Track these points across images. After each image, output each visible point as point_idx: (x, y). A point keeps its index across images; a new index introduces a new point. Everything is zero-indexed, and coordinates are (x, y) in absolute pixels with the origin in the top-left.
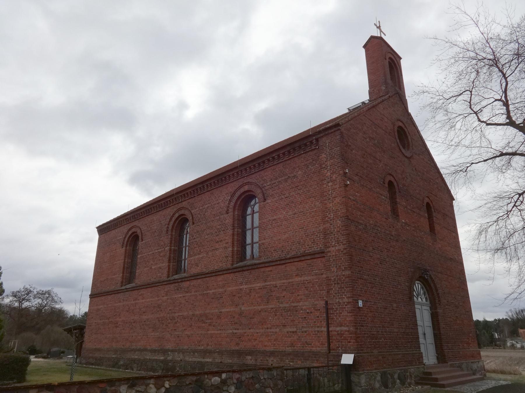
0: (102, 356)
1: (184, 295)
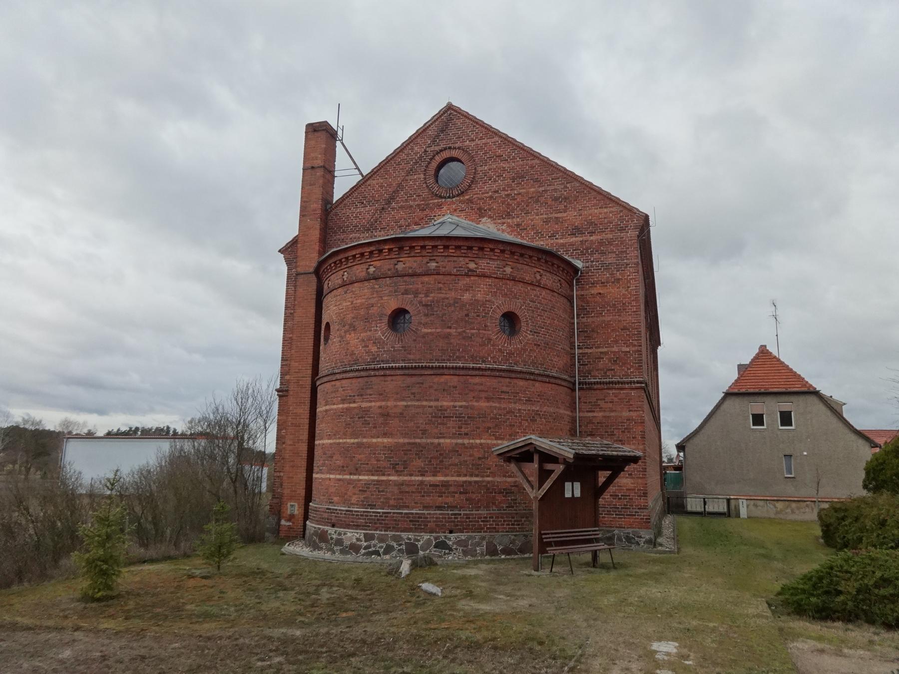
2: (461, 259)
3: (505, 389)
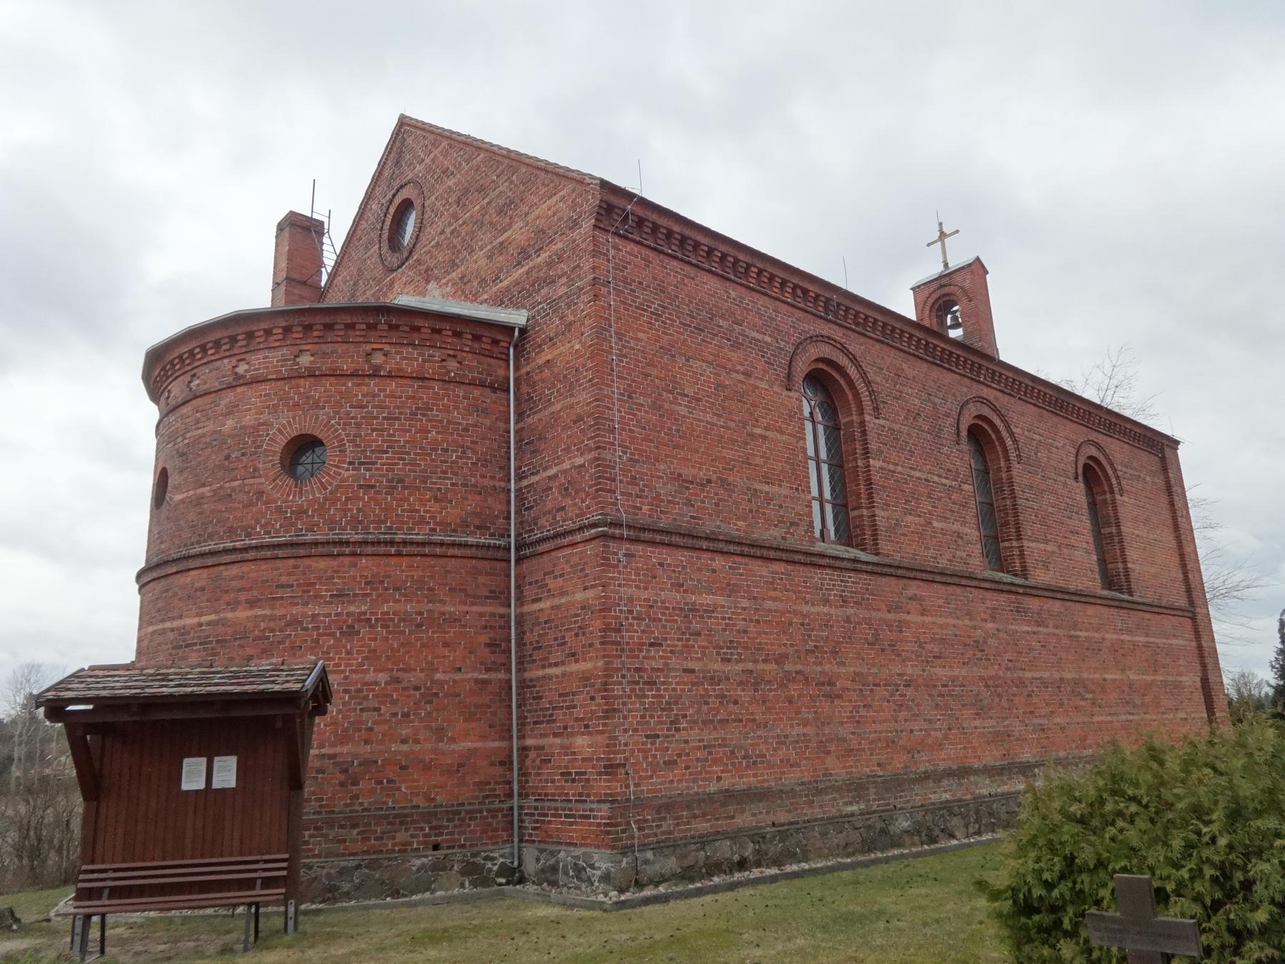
0: (783, 817)
1: (1036, 629)
2: (226, 361)
3: (284, 579)
